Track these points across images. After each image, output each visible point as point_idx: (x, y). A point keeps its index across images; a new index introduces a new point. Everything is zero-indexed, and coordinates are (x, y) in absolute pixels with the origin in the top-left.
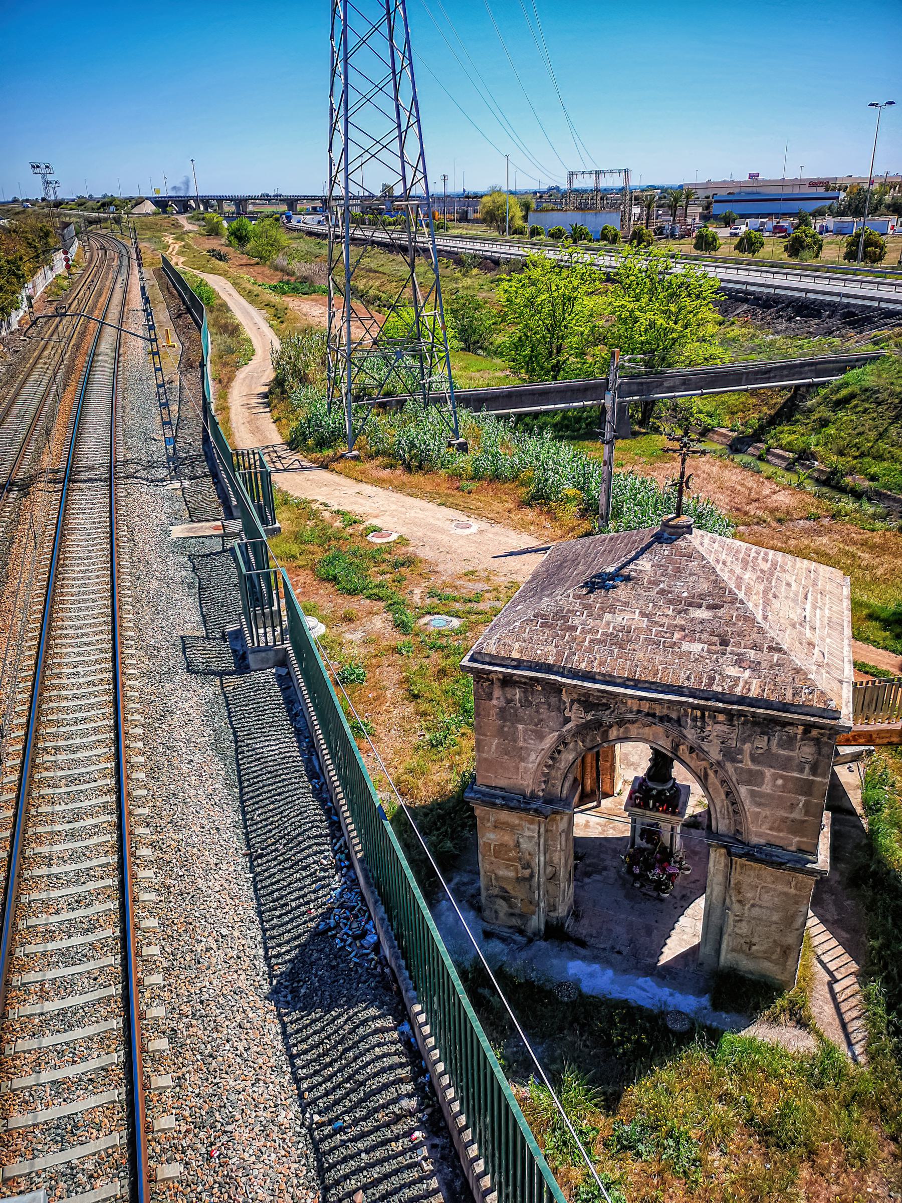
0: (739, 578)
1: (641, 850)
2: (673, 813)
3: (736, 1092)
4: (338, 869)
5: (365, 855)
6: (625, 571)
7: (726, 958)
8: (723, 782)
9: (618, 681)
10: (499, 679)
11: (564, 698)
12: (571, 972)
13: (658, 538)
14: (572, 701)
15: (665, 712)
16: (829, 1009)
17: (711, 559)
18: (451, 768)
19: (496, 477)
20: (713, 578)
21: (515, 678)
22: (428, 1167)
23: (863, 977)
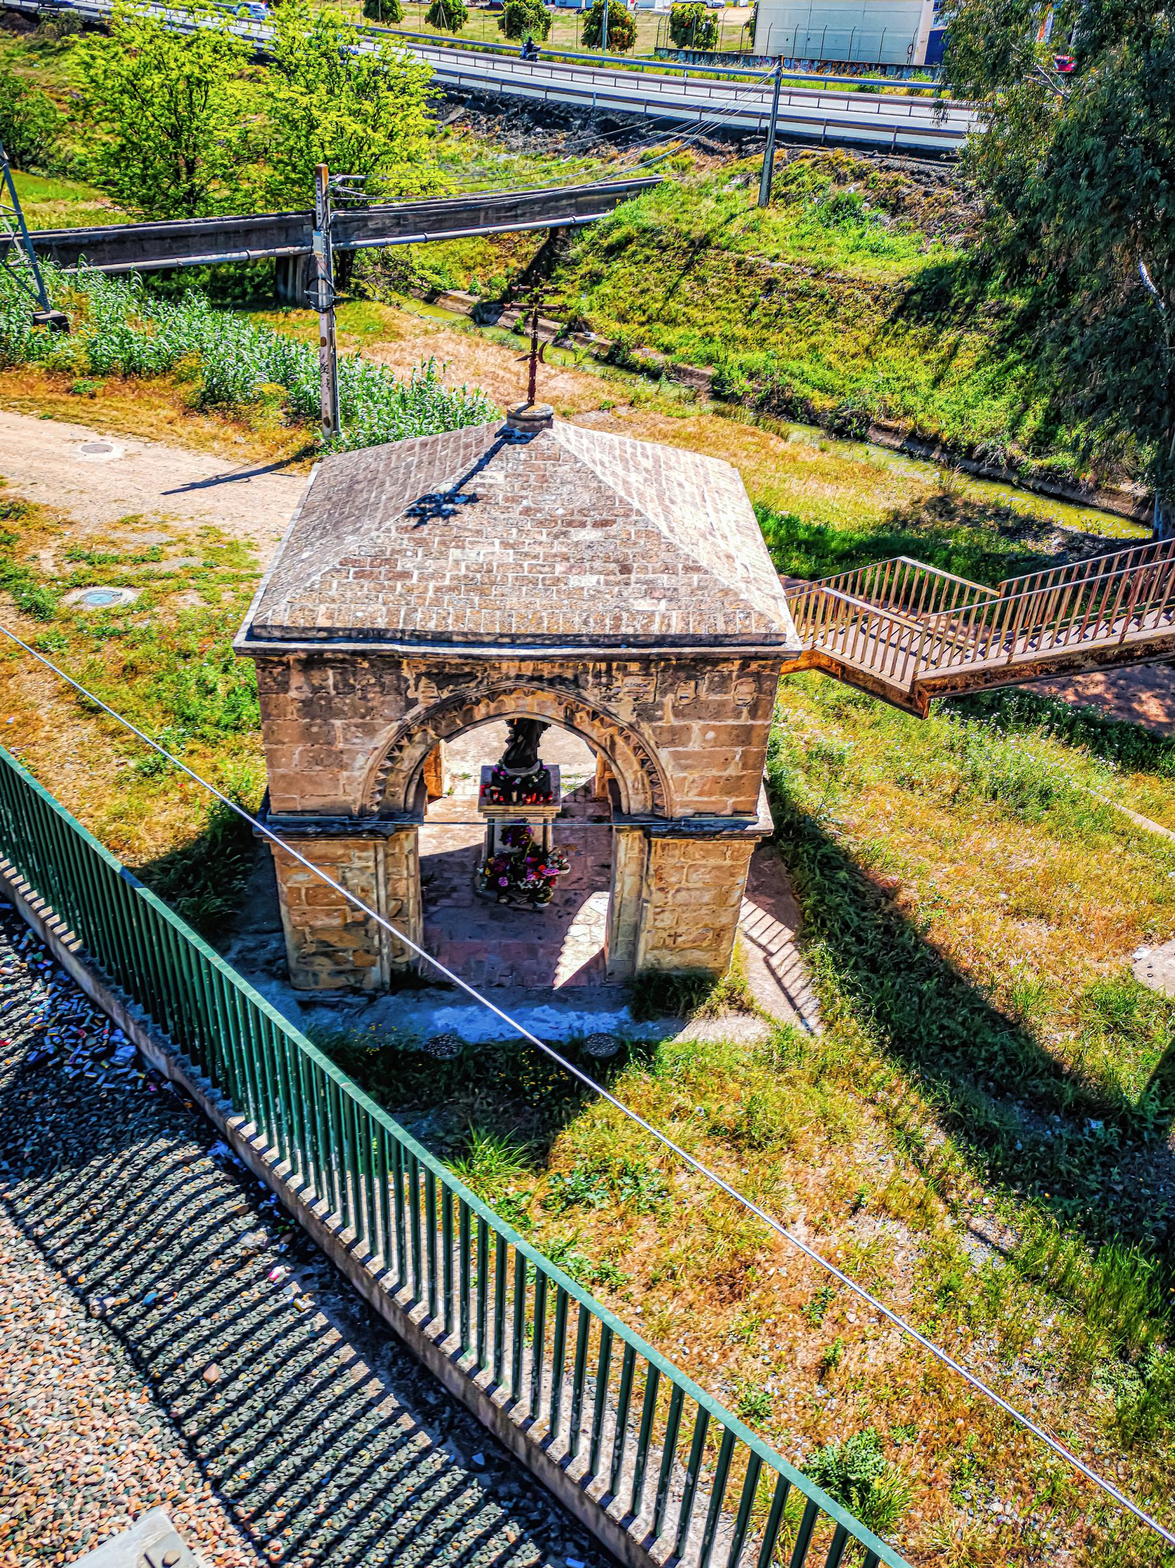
0: (625, 482)
1: (504, 857)
2: (547, 803)
3: (688, 1104)
4: (34, 974)
5: (85, 945)
6: (467, 490)
7: (644, 958)
8: (637, 749)
9: (487, 639)
10: (298, 661)
11: (406, 673)
12: (440, 1024)
13: (507, 436)
14: (418, 677)
15: (557, 671)
16: (771, 986)
17: (585, 458)
18: (184, 801)
19: (132, 370)
20: (595, 484)
21: (329, 655)
22: (306, 1303)
23: (802, 940)
